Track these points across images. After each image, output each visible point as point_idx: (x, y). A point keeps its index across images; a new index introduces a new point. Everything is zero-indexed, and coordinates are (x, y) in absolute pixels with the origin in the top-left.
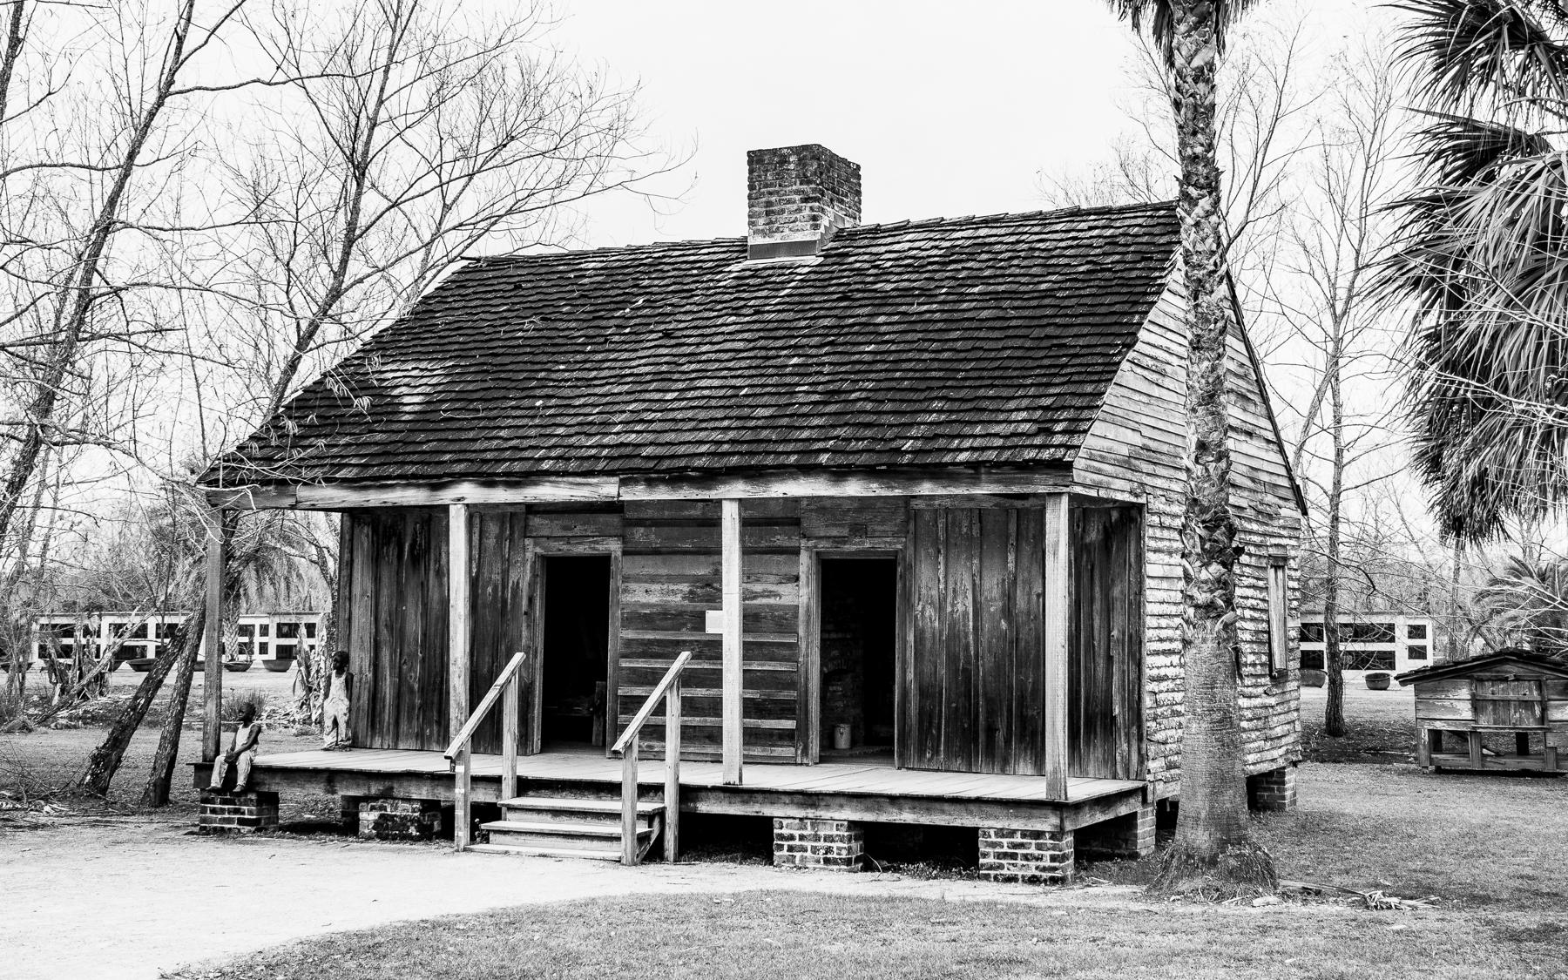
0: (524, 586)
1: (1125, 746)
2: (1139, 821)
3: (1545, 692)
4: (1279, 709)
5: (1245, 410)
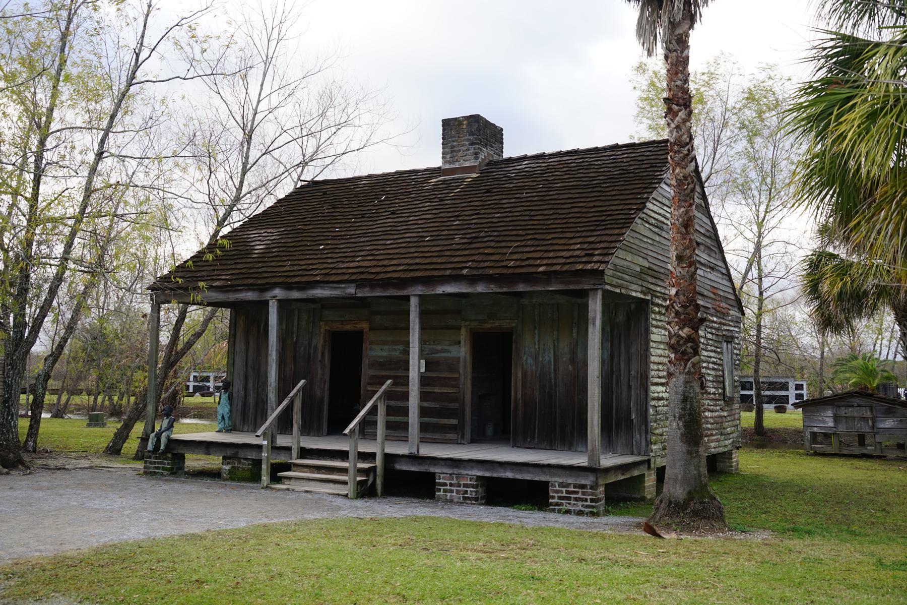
0: (320, 347)
1: (638, 436)
2: (646, 479)
3: (874, 413)
4: (729, 418)
5: (709, 255)
